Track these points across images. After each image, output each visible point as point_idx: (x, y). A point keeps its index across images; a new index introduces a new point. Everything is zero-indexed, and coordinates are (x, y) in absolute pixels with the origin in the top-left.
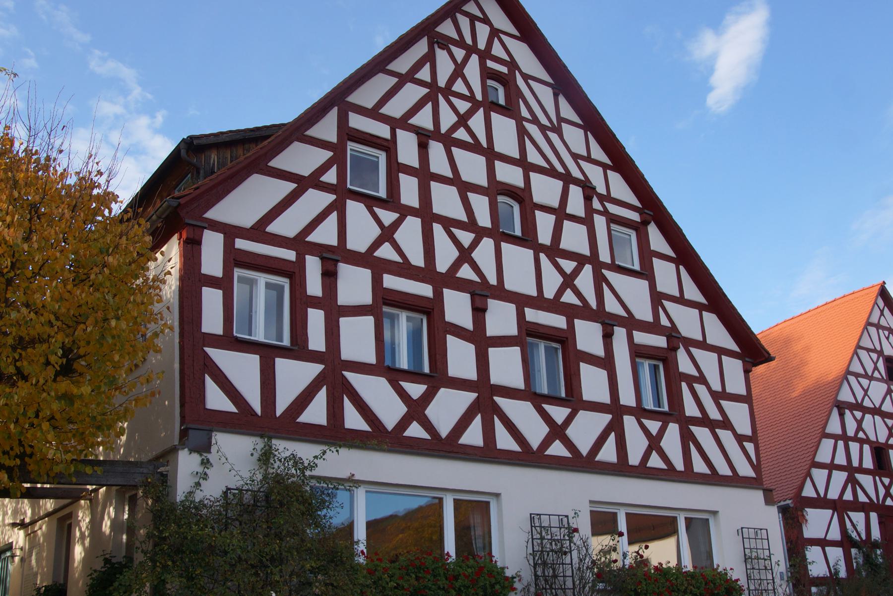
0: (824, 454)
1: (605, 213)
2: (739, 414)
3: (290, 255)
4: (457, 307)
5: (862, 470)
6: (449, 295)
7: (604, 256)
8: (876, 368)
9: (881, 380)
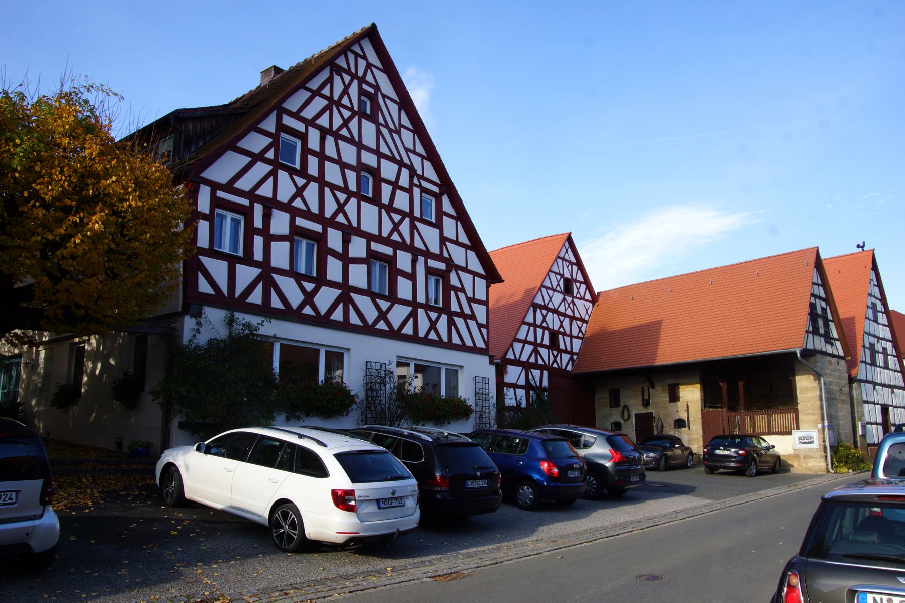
0: (521, 335)
1: (420, 186)
2: (480, 312)
3: (246, 202)
4: (335, 239)
5: (542, 345)
6: (330, 231)
7: (417, 214)
8: (558, 285)
9: (560, 292)
